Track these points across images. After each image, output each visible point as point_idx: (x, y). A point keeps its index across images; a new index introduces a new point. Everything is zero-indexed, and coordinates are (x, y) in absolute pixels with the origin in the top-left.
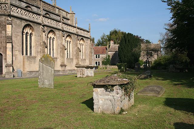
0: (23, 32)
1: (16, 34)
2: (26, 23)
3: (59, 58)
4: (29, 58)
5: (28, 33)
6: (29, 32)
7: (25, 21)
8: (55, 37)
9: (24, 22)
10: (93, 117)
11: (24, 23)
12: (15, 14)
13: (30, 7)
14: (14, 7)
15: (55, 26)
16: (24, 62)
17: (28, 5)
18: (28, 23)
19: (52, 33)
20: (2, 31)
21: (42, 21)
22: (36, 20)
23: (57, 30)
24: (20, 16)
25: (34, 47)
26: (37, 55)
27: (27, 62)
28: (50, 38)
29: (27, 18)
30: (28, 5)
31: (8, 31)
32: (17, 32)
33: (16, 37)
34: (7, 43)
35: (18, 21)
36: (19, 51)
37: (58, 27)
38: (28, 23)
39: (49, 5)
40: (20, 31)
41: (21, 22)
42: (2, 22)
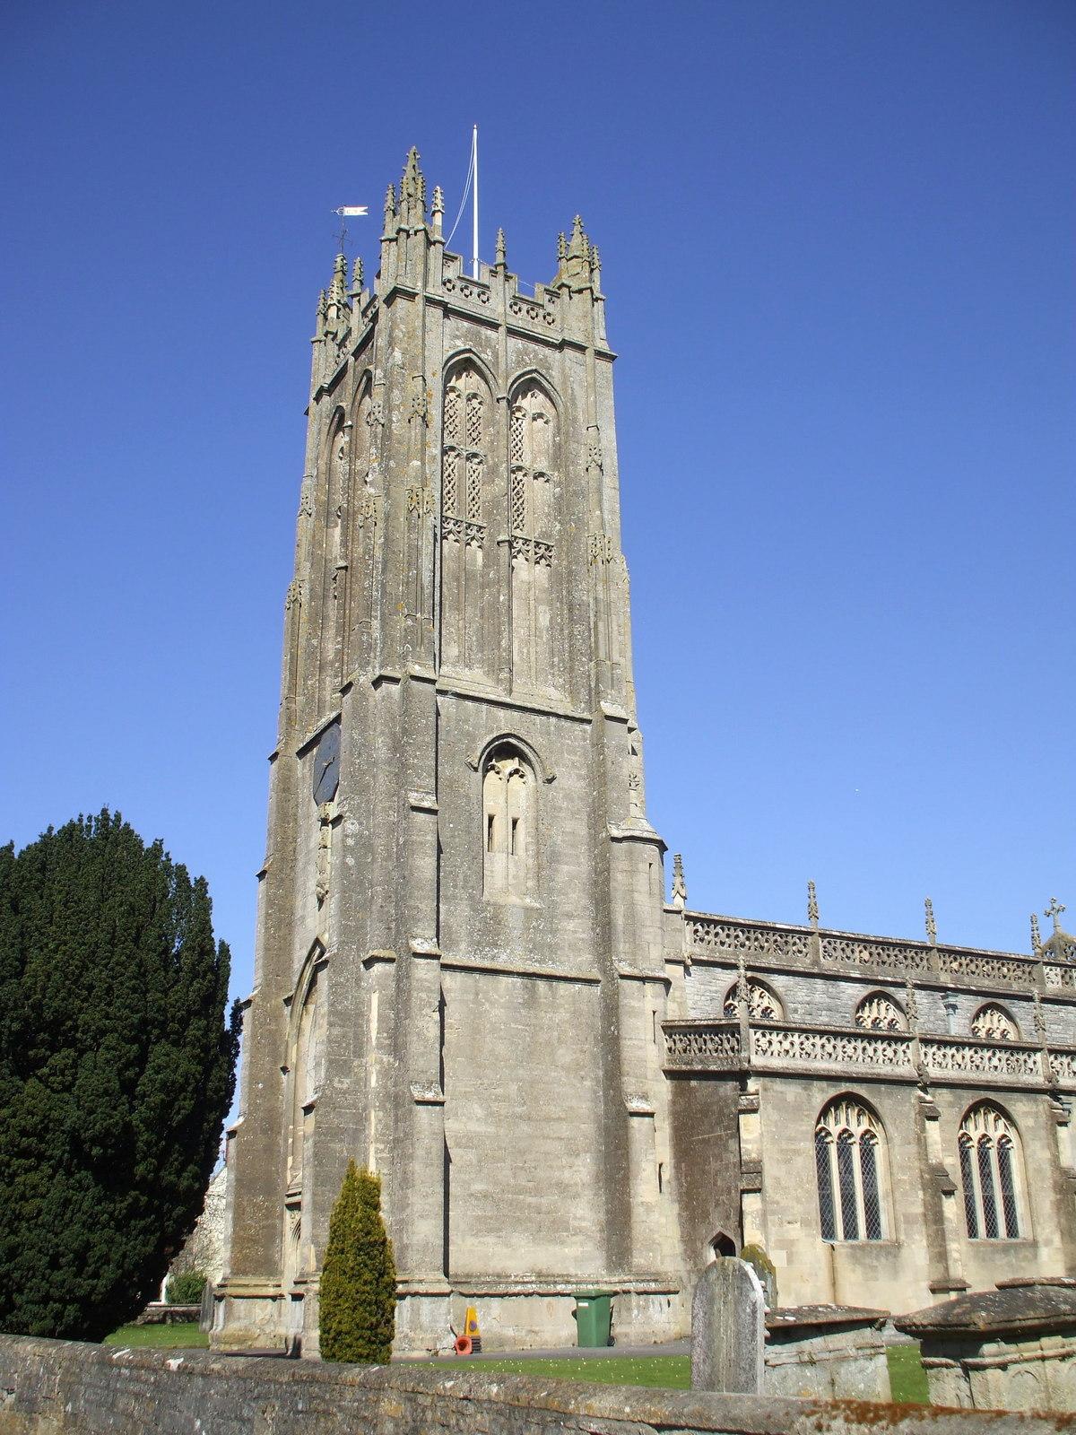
0: (821, 1137)
1: (784, 1147)
2: (833, 1091)
3: (1048, 1243)
4: (859, 1253)
5: (851, 1136)
6: (991, 1133)
7: (824, 1084)
8: (1012, 1134)
9: (822, 1090)
10: (342, 943)
11: (821, 1094)
12: (777, 1063)
13: (888, 997)
14: (768, 1035)
15: (1003, 1077)
16: (833, 1270)
17: (878, 988)
18: (845, 1088)
19: (992, 1116)
20: (727, 1141)
21: (920, 1067)
22: (885, 1070)
23: (1016, 1095)
24: (800, 1064)
25: (884, 1198)
26: (906, 1234)
27: (854, 1271)
28: (845, 1135)
29: (835, 1067)
30: (878, 988)
31: (747, 1141)
32: (790, 1139)
33: (788, 1161)
34: (744, 1192)
35: (792, 1090)
36: (806, 1223)
37: (1027, 1079)
38: (845, 1088)
39: (999, 958)
40: (807, 1132)
41: (805, 1089)
42: (725, 1101)
